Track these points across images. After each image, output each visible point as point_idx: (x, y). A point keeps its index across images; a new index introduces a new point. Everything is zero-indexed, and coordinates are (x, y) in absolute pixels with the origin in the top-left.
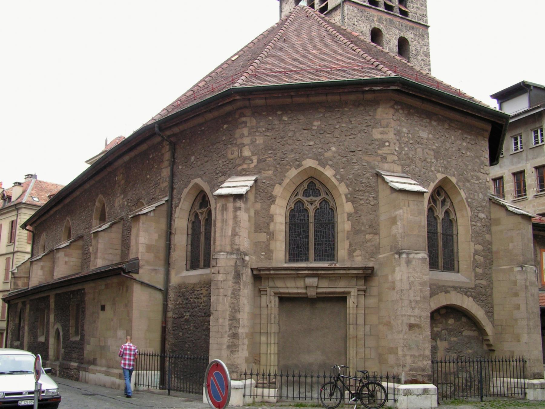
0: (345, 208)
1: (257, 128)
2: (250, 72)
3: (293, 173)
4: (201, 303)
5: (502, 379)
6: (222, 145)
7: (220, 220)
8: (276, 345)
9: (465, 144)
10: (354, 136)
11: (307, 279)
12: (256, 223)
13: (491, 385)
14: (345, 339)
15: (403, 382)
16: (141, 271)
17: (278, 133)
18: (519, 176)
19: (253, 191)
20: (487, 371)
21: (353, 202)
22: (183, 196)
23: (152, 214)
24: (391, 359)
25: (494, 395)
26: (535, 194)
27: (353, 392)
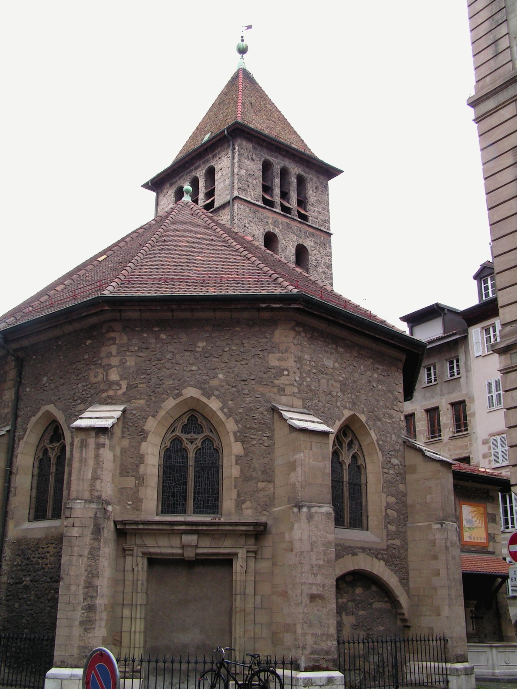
0: (232, 449)
1: (128, 346)
2: (122, 278)
3: (170, 403)
4: (47, 564)
5: (416, 663)
6: (84, 365)
7: (77, 460)
8: (143, 620)
9: (376, 375)
10: (247, 362)
11: (184, 536)
12: (122, 464)
13: (408, 671)
14: (230, 612)
15: (303, 669)
17: (153, 353)
18: (433, 413)
19: (121, 424)
20: (403, 652)
21: (243, 442)
22: (30, 426)
24: (288, 639)
25: (411, 684)
26: (451, 435)
27: (240, 682)
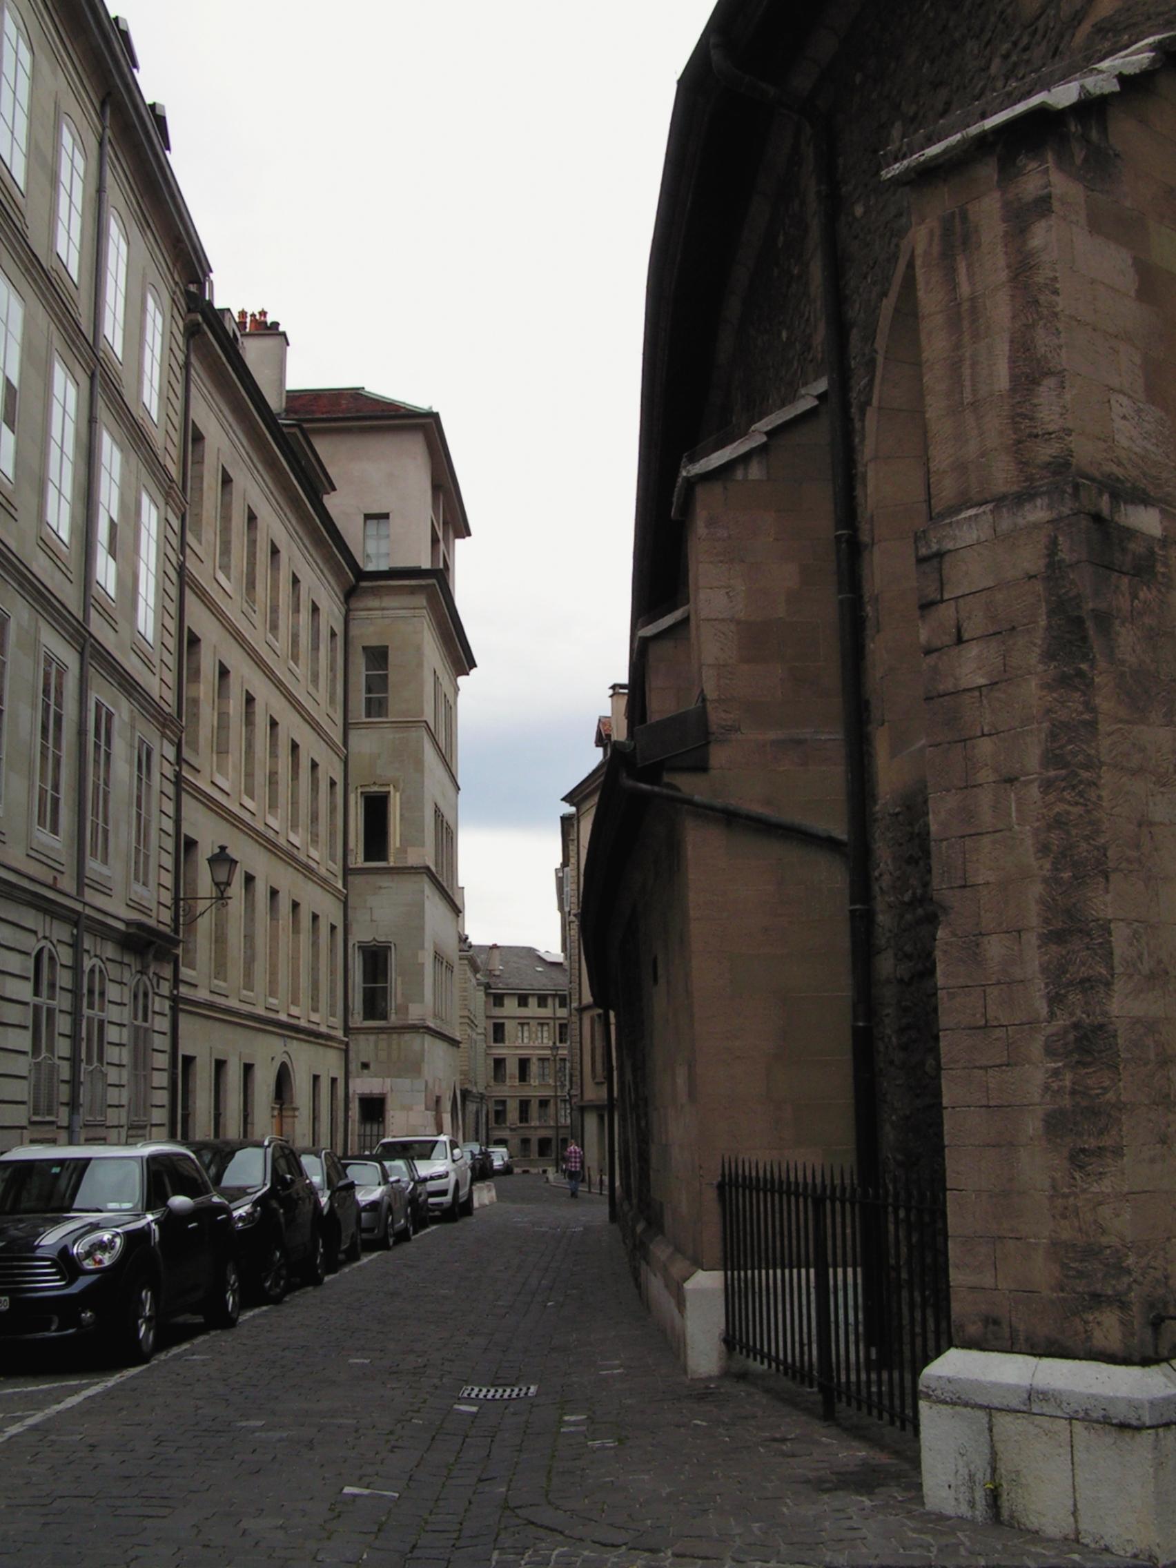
16: (719, 756)
23: (755, 471)
